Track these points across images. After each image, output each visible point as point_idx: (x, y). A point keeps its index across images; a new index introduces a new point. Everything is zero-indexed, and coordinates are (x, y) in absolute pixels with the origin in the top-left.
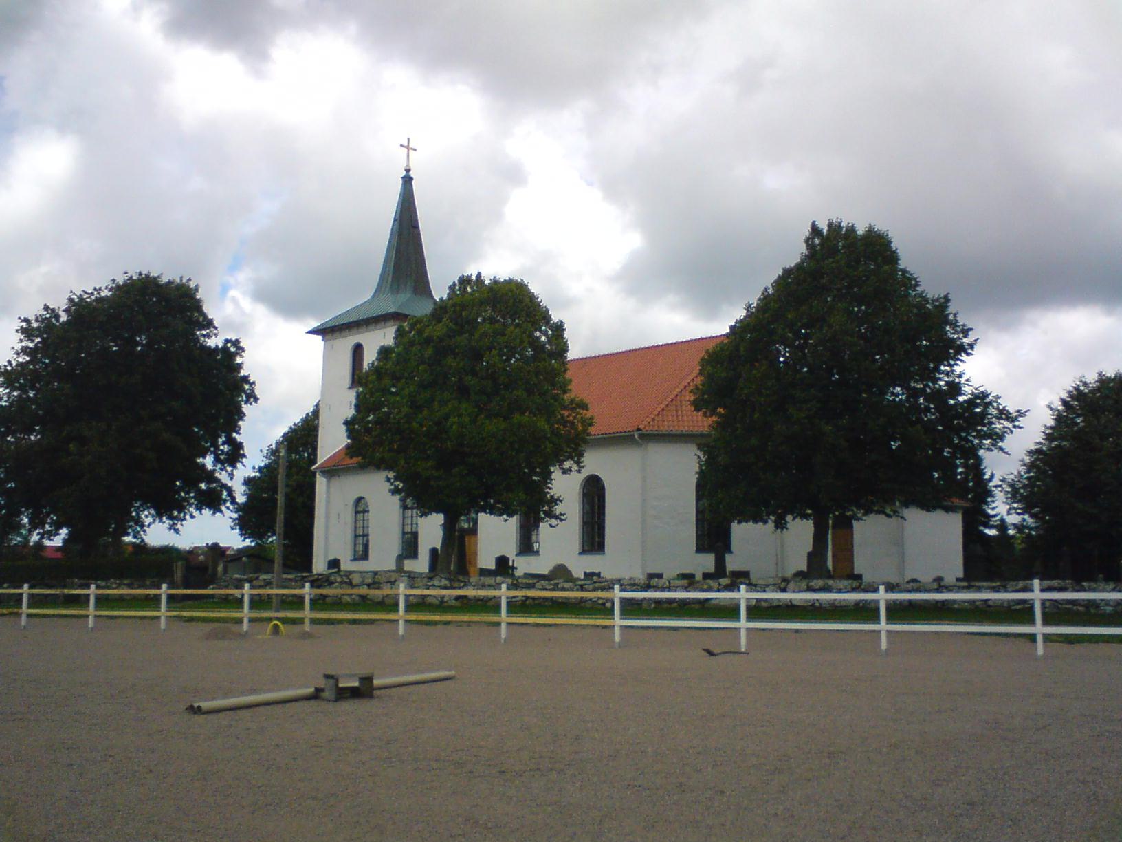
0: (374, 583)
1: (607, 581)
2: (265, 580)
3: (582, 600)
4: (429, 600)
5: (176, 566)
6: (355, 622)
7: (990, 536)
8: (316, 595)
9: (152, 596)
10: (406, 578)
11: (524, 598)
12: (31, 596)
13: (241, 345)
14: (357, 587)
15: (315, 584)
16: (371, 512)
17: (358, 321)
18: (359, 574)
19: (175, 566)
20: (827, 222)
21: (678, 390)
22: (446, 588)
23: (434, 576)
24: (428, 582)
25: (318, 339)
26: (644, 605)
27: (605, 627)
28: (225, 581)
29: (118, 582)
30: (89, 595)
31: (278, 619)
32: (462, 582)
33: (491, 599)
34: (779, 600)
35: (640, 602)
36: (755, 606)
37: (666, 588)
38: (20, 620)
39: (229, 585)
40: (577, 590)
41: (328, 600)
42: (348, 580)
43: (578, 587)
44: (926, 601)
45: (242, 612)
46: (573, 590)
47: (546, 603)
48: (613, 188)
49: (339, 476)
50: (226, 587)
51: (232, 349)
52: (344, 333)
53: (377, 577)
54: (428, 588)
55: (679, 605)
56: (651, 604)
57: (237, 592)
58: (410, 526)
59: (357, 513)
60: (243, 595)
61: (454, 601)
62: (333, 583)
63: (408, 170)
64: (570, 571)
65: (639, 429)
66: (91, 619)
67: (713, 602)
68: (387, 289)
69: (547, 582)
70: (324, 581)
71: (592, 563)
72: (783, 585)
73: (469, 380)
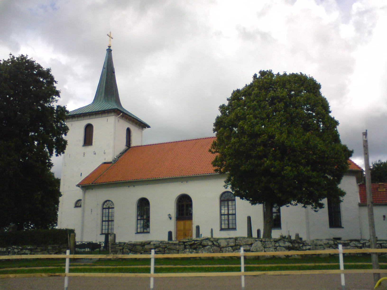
0: (236, 245)
15: (193, 247)
18: (224, 240)
29: (20, 248)
39: (123, 248)
42: (217, 244)
49: (92, 189)
59: (103, 208)
62: (206, 246)
68: (102, 98)
71: (336, 232)
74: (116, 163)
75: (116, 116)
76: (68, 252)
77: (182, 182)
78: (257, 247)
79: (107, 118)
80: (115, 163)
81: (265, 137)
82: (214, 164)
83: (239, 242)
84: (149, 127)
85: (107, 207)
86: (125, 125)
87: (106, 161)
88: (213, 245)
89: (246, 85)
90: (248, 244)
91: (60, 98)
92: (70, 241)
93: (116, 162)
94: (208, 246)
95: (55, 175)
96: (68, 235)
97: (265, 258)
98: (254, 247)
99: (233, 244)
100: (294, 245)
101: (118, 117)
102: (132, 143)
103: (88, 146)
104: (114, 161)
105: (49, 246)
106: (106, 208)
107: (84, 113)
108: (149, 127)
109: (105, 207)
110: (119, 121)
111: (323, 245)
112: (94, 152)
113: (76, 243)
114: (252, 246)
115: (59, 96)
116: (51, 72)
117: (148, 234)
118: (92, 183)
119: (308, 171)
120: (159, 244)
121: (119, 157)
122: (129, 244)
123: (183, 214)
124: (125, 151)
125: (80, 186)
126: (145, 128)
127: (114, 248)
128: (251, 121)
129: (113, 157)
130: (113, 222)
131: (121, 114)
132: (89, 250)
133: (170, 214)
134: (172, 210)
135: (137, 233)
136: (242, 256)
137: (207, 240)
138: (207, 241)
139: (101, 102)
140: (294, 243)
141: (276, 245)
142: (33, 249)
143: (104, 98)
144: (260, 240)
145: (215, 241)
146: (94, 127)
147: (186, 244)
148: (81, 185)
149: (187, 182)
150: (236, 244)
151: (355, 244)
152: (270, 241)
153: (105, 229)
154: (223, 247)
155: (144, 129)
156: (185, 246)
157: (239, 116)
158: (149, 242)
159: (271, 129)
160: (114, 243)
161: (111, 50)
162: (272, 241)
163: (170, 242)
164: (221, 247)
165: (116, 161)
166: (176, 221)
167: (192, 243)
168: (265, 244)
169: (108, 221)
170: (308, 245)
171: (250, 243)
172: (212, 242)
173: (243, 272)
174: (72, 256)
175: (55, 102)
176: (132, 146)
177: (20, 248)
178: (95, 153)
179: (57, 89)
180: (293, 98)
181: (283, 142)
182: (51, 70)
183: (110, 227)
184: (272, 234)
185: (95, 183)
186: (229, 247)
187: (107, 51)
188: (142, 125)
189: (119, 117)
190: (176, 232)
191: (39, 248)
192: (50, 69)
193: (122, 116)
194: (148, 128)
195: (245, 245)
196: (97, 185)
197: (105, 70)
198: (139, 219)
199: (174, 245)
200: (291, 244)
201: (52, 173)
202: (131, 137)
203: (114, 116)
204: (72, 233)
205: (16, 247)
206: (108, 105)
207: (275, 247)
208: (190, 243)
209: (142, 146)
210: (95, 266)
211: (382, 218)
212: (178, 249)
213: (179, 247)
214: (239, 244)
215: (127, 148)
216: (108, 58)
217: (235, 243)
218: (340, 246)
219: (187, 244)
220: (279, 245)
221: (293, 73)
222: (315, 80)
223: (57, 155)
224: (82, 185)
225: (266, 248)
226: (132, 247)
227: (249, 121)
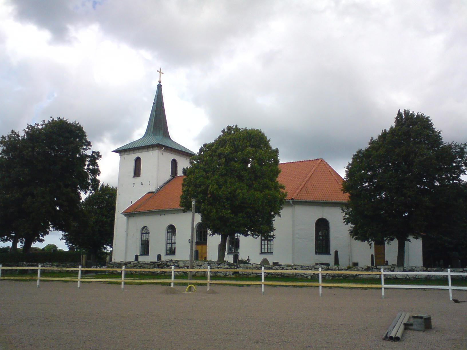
2: (134, 264)
4: (219, 274)
5: (82, 256)
6: (294, 286)
7: (67, 252)
8: (161, 272)
9: (70, 271)
10: (207, 264)
12: (82, 271)
13: (100, 154)
14: (182, 268)
16: (150, 233)
17: (139, 147)
18: (182, 262)
19: (82, 257)
20: (403, 111)
21: (304, 182)
22: (227, 268)
23: (221, 263)
24: (218, 266)
25: (117, 155)
28: (112, 264)
29: (51, 264)
30: (78, 271)
31: (191, 283)
32: (236, 266)
34: (390, 275)
35: (325, 276)
36: (379, 278)
37: (337, 270)
38: (36, 283)
39: (114, 266)
41: (166, 274)
42: (177, 265)
43: (294, 269)
44: (457, 276)
45: (121, 279)
48: (197, 102)
49: (134, 217)
50: (113, 267)
51: (96, 156)
54: (218, 268)
55: (343, 278)
56: (330, 277)
57: (119, 270)
58: (171, 240)
59: (142, 233)
60: (122, 271)
61: (231, 275)
63: (160, 82)
64: (268, 262)
65: (292, 199)
66: (79, 283)
67: (359, 276)
69: (278, 267)
72: (392, 269)
73: (243, 173)
76: (40, 266)
79: (151, 152)
110: (125, 158)
120: (137, 264)
121: (162, 187)
137: (170, 262)
139: (150, 136)
140: (231, 265)
141: (218, 267)
142: (58, 265)
143: (153, 132)
144: (208, 262)
145: (176, 263)
147: (155, 264)
151: (276, 268)
152: (215, 264)
162: (216, 264)
165: (158, 191)
176: (179, 176)
177: (51, 264)
183: (269, 246)
185: (134, 212)
186: (185, 267)
191: (62, 264)
198: (263, 240)
202: (177, 167)
205: (48, 263)
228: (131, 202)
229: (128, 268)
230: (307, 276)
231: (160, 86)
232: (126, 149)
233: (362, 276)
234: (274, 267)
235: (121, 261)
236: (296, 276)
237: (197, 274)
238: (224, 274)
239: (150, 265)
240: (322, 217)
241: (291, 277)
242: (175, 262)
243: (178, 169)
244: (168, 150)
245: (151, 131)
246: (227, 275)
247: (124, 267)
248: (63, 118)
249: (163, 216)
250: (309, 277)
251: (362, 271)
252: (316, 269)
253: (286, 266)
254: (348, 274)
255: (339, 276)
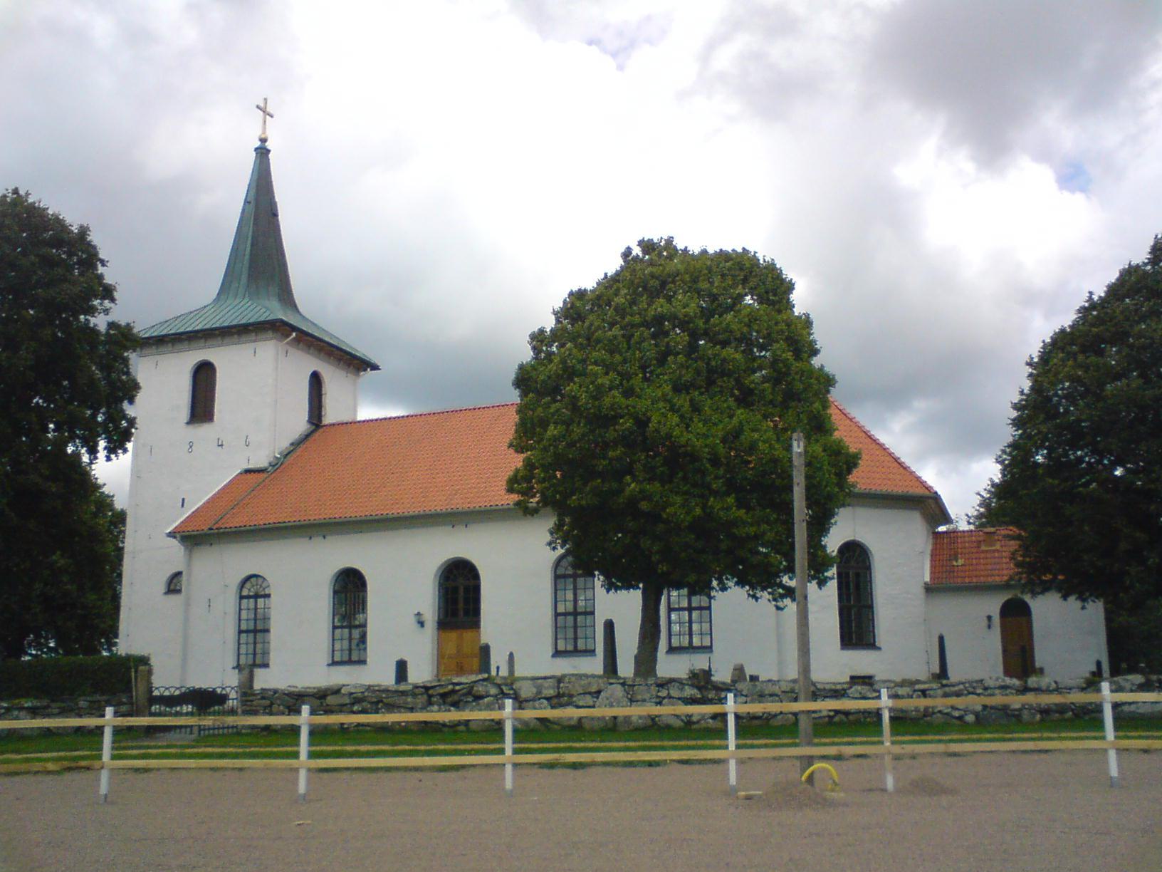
0: (559, 696)
1: (963, 683)
3: (927, 713)
11: (832, 714)
12: (118, 731)
15: (449, 700)
18: (529, 682)
26: (1026, 715)
27: (1095, 750)
33: (775, 716)
35: (1016, 713)
39: (272, 704)
40: (919, 697)
42: (511, 692)
43: (919, 693)
46: (912, 697)
47: (868, 720)
52: (179, 346)
53: (562, 685)
59: (242, 597)
61: (710, 721)
62: (481, 697)
63: (263, 140)
70: (464, 695)
71: (861, 661)
74: (278, 470)
75: (281, 341)
76: (109, 711)
77: (453, 526)
78: (613, 700)
79: (253, 345)
80: (275, 470)
81: (627, 424)
82: (513, 484)
83: (566, 687)
84: (375, 367)
85: (251, 594)
86: (305, 364)
87: (251, 466)
88: (501, 696)
89: (606, 274)
90: (590, 693)
91: (116, 304)
92: (136, 686)
93: (277, 469)
94: (488, 696)
95: (115, 502)
96: (133, 670)
97: (631, 727)
98: (605, 699)
99: (551, 692)
100: (705, 693)
101: (287, 343)
102: (326, 414)
103: (201, 424)
104: (274, 466)
105: (80, 700)
106: (248, 597)
107: (191, 332)
108: (375, 367)
109: (245, 593)
111: (780, 693)
112: (219, 439)
113: (152, 692)
114: (600, 697)
115: (113, 300)
116: (89, 235)
117: (362, 667)
118: (211, 529)
119: (728, 509)
121: (287, 455)
122: (285, 694)
123: (454, 613)
124: (304, 437)
125: (178, 535)
126: (365, 370)
127: (249, 703)
128: (596, 383)
129: (272, 455)
130: (266, 634)
131: (294, 334)
132: (193, 708)
133: (421, 613)
134: (426, 600)
135: (334, 663)
136: (509, 718)
137: (485, 683)
138: (486, 686)
139: (238, 301)
141: (659, 694)
144: (621, 681)
145: (506, 685)
146: (218, 370)
147: (431, 692)
148: (179, 532)
149: (466, 526)
150: (559, 693)
151: (860, 693)
153: (247, 654)
154: (527, 701)
155: (362, 373)
156: (430, 696)
157: (570, 367)
158: (336, 688)
159: (642, 405)
160: (249, 691)
161: (269, 151)
163: (402, 687)
164: (521, 700)
166: (436, 632)
167: (446, 690)
168: (633, 691)
169: (255, 631)
170: (743, 695)
171: (594, 689)
172: (499, 686)
173: (509, 757)
174: (121, 721)
175: (102, 314)
176: (326, 423)
178: (222, 442)
179: (108, 280)
180: (713, 317)
181: (669, 436)
182: (90, 231)
184: (657, 667)
186: (542, 700)
187: (257, 154)
188: (357, 364)
189: (287, 343)
190: (436, 658)
191: (53, 705)
192: (89, 228)
193: (298, 341)
194: (371, 370)
195: (581, 694)
196: (223, 533)
197: (251, 208)
199: (400, 694)
200: (698, 693)
201: (108, 496)
202: (323, 396)
203: (273, 342)
204: (142, 665)
206: (258, 308)
207: (658, 700)
208: (442, 691)
209: (344, 425)
210: (194, 747)
211: (985, 622)
212: (410, 706)
213: (414, 700)
214: (567, 692)
215: (311, 429)
216: (259, 173)
217: (556, 690)
218: (509, 703)
219: (435, 693)
220: (669, 694)
221: (721, 250)
222: (777, 269)
223: (108, 459)
224: (184, 534)
225: (634, 701)
226: (294, 701)
227: (592, 383)
228: (181, 500)
229: (329, 711)
230: (962, 713)
231: (264, 151)
232: (164, 336)
233: (1133, 708)
234: (853, 689)
235: (289, 686)
236: (925, 716)
237: (587, 725)
238: (684, 718)
239: (414, 695)
240: (852, 538)
241: (911, 719)
242: (503, 681)
243: (327, 401)
244: (301, 345)
245: (242, 283)
246: (694, 723)
247: (305, 709)
248: (28, 194)
249: (318, 541)
250: (970, 718)
251: (1132, 691)
252: (989, 691)
253: (892, 685)
254: (1091, 703)
255: (1062, 709)
